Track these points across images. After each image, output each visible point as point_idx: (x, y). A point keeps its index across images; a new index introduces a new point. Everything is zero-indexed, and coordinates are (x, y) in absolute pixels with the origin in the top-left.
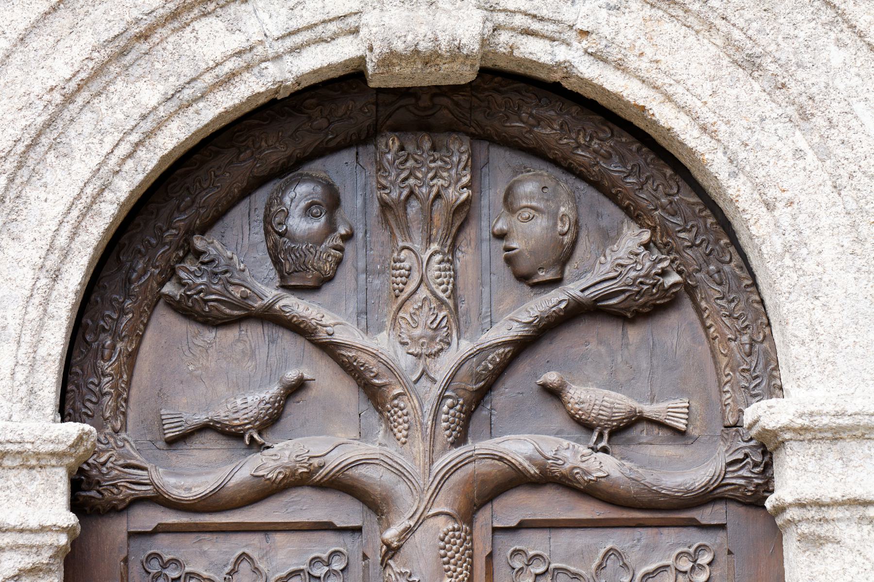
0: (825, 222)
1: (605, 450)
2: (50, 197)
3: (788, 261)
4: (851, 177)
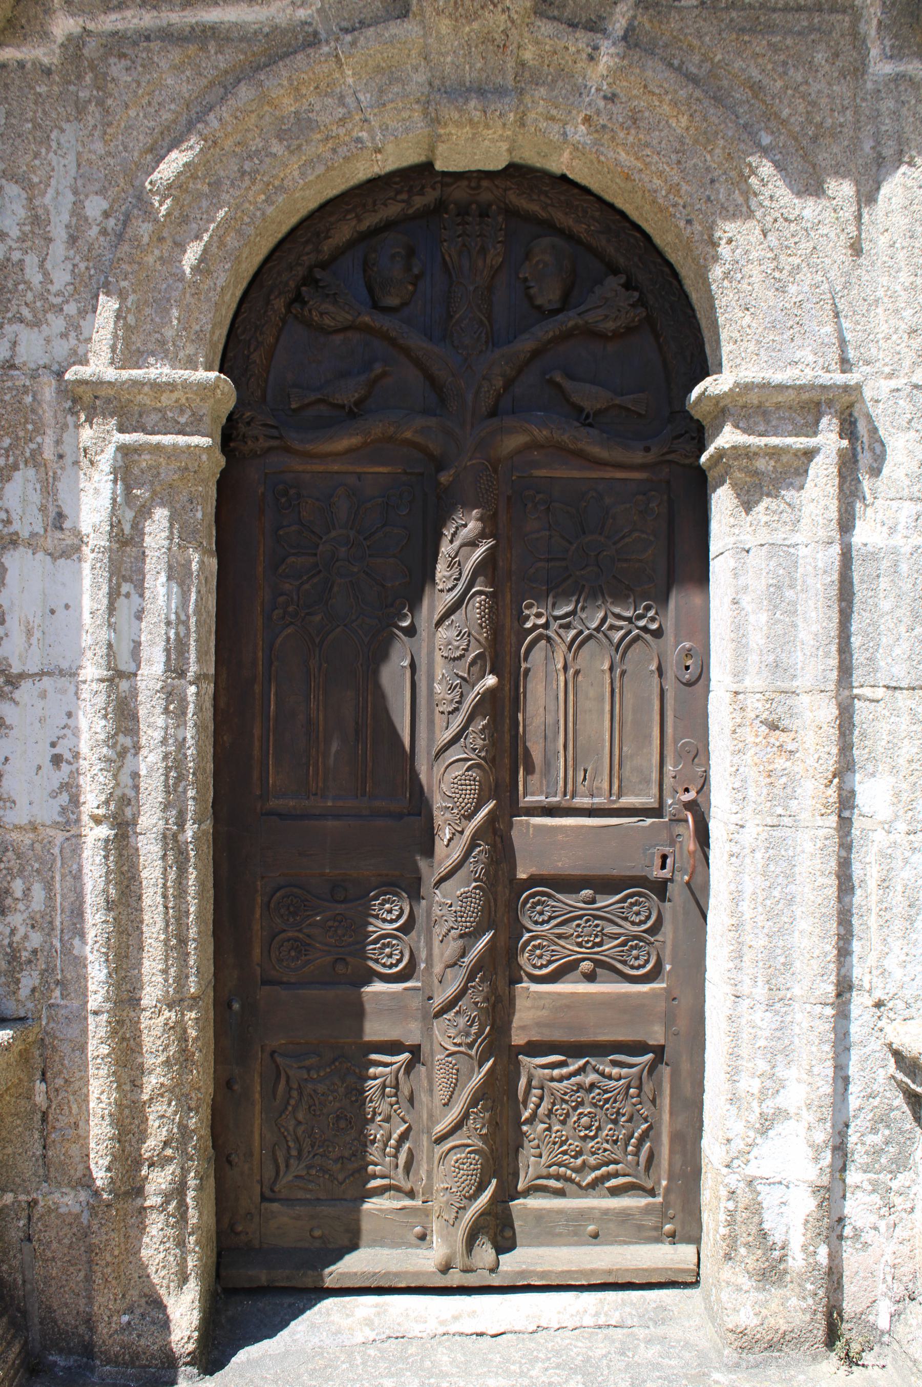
0: (754, 255)
1: (590, 425)
2: (205, 216)
3: (726, 283)
4: (776, 220)
